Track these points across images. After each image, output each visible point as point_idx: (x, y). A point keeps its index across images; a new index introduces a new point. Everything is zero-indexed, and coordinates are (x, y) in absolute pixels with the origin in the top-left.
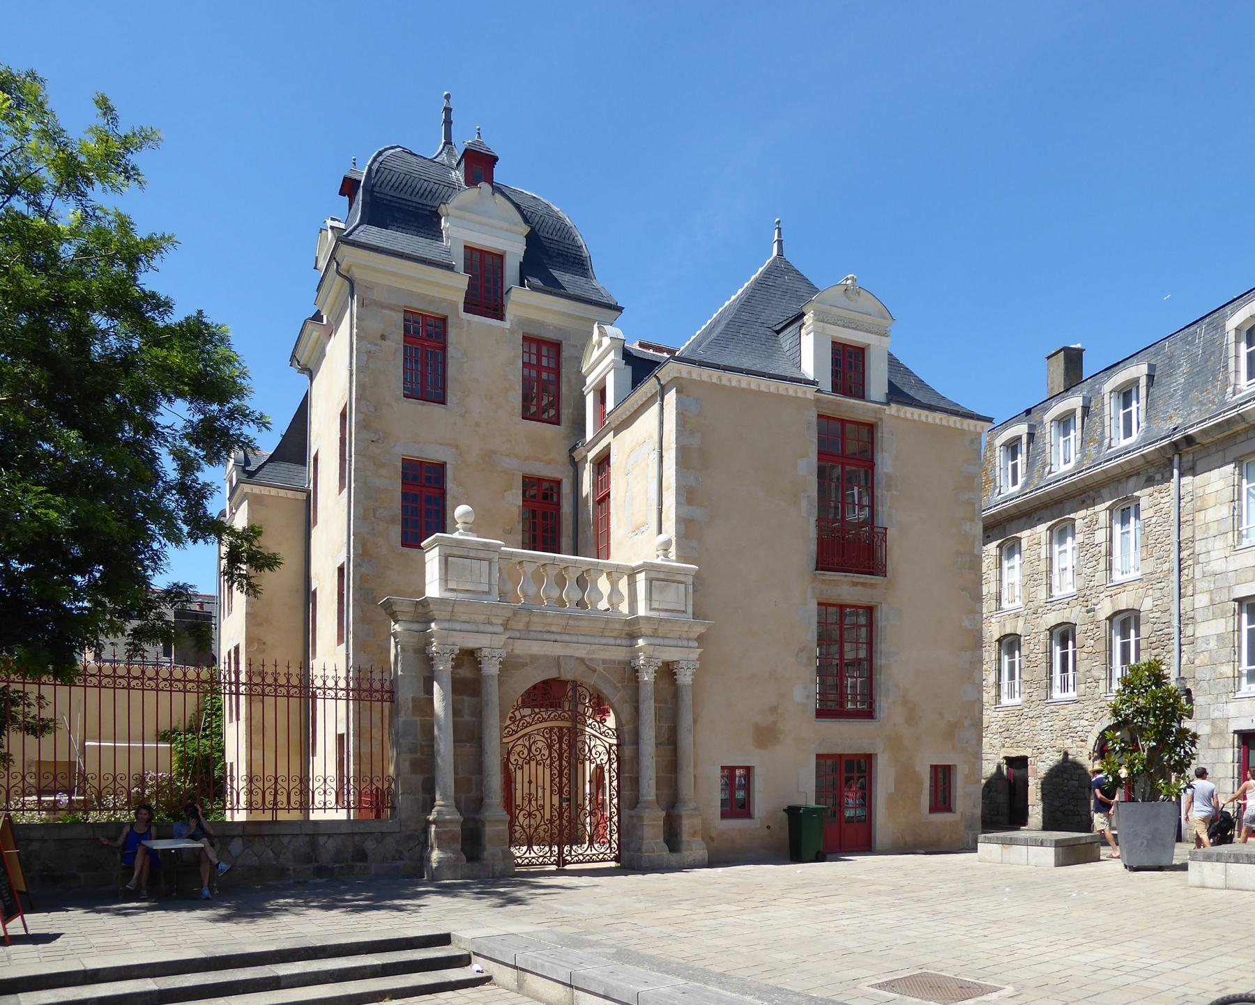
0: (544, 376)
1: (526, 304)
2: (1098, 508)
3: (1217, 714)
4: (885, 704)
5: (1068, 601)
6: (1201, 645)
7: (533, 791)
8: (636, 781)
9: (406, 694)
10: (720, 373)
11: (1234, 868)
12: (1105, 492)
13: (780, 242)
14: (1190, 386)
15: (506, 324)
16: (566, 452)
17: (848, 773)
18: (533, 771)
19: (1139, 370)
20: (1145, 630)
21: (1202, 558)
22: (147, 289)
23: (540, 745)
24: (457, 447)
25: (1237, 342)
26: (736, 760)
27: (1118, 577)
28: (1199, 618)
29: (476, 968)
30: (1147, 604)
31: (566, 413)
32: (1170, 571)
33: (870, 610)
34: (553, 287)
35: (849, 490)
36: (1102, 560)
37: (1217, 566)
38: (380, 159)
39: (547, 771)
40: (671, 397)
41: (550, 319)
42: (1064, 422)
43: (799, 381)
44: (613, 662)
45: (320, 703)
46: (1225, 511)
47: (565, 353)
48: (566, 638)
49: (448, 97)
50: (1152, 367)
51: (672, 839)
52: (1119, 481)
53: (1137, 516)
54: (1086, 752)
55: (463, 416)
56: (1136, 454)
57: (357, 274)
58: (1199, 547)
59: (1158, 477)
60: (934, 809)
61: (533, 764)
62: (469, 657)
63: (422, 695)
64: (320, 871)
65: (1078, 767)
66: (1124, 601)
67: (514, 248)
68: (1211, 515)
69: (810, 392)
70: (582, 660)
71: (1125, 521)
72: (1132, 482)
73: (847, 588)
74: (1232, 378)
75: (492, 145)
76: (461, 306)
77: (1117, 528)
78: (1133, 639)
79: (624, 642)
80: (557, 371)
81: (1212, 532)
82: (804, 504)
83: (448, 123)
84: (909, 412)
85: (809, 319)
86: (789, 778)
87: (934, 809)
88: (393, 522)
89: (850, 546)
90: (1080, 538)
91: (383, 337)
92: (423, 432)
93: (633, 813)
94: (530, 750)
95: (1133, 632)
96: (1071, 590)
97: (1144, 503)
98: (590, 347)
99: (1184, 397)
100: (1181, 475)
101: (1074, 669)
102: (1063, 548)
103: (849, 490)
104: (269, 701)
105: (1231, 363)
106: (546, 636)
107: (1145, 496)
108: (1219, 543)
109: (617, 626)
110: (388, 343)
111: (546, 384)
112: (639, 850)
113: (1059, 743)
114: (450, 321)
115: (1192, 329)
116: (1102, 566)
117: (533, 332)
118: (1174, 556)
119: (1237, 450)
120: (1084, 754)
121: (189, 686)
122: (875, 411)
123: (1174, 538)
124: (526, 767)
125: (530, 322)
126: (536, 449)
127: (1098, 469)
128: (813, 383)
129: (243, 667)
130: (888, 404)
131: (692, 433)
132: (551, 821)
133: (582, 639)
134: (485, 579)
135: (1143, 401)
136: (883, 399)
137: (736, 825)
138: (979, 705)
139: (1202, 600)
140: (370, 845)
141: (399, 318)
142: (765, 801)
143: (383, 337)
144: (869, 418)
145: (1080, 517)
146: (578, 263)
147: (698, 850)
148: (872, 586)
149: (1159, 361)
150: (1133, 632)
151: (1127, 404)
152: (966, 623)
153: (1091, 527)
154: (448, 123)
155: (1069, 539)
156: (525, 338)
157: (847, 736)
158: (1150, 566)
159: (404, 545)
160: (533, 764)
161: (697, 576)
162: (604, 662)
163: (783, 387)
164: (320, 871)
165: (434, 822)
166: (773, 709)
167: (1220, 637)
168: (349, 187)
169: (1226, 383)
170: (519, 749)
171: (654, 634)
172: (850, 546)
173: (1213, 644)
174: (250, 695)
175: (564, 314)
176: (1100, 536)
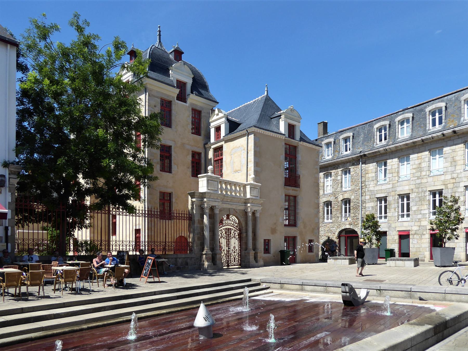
0: (196, 120)
1: (194, 99)
2: (338, 170)
5: (330, 195)
6: (367, 209)
8: (246, 244)
9: (197, 218)
10: (264, 131)
11: (397, 262)
12: (340, 166)
13: (267, 91)
14: (364, 140)
15: (187, 105)
16: (203, 145)
17: (291, 241)
19: (350, 134)
20: (352, 204)
21: (367, 186)
24: (175, 141)
25: (377, 132)
27: (344, 189)
28: (367, 202)
29: (263, 286)
30: (352, 197)
31: (203, 132)
32: (359, 189)
33: (295, 197)
34: (200, 95)
35: (290, 165)
36: (340, 184)
37: (371, 189)
38: (152, 50)
40: (252, 137)
41: (199, 104)
42: (328, 145)
43: (278, 133)
44: (241, 210)
46: (374, 175)
47: (203, 114)
48: (231, 203)
49: (159, 27)
50: (353, 134)
51: (256, 258)
52: (345, 163)
53: (350, 173)
54: (335, 237)
56: (350, 157)
57: (148, 86)
58: (367, 183)
59: (356, 164)
60: (309, 252)
62: (212, 209)
63: (201, 218)
64: (178, 268)
65: (332, 241)
66: (346, 196)
67: (189, 82)
68: (370, 175)
69: (283, 137)
70: (234, 209)
71: (346, 174)
72: (348, 164)
73: (291, 191)
74: (376, 140)
76: (176, 98)
77: (343, 176)
78: (348, 206)
79: (244, 204)
81: (371, 179)
84: (305, 144)
85: (283, 117)
86: (278, 244)
87: (309, 252)
88: (158, 163)
89: (292, 180)
90: (333, 178)
91: (155, 106)
93: (246, 252)
95: (348, 204)
96: (329, 192)
97: (351, 170)
98: (213, 115)
99: (363, 143)
100: (362, 164)
101: (331, 214)
102: (327, 180)
103: (290, 165)
105: (375, 136)
106: (227, 203)
107: (352, 168)
108: (372, 183)
109: (243, 200)
110: (156, 108)
111: (199, 124)
112: (249, 262)
113: (327, 234)
114: (173, 102)
115: (364, 125)
116: (340, 186)
117: (195, 107)
118: (360, 185)
119: (377, 159)
120: (334, 238)
122: (297, 143)
123: (360, 180)
125: (194, 104)
126: (195, 143)
127: (339, 160)
128: (284, 135)
129: (146, 209)
130: (300, 141)
131: (257, 147)
132: (226, 254)
133: (234, 203)
135: (351, 143)
136: (299, 140)
137: (267, 255)
138: (318, 223)
139: (367, 197)
140: (189, 261)
141: (159, 100)
142: (274, 248)
143: (155, 106)
144: (295, 145)
145: (333, 172)
146: (205, 87)
147: (261, 262)
148: (297, 191)
149: (355, 132)
150: (348, 204)
151: (346, 142)
152: (316, 201)
153: (336, 175)
155: (329, 178)
156: (192, 109)
158: (353, 187)
159: (161, 171)
161: (261, 187)
162: (239, 210)
163: (271, 134)
164: (178, 268)
165: (205, 254)
166: (275, 224)
167: (372, 207)
169: (374, 142)
171: (252, 203)
172: (292, 180)
173: (370, 209)
174: (148, 217)
175: (204, 103)
176: (339, 178)
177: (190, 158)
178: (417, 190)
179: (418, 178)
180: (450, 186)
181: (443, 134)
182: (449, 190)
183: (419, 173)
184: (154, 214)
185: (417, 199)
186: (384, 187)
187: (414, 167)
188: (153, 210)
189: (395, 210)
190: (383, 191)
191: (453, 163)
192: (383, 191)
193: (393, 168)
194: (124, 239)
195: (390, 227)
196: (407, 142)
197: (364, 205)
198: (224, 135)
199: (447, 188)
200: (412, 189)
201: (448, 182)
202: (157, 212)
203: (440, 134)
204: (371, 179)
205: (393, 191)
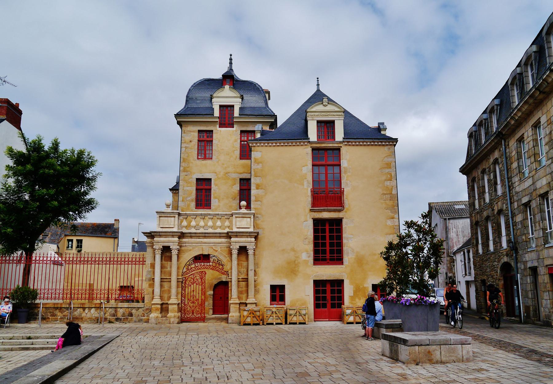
7: (195, 294)
22: (63, 150)
23: (198, 278)
26: (277, 282)
39: (200, 287)
45: (33, 265)
55: (218, 162)
61: (195, 284)
64: (118, 320)
88: (192, 201)
92: (203, 169)
94: (194, 280)
104: (11, 265)
124: (192, 286)
134: (172, 223)
140: (134, 311)
143: (191, 141)
157: (328, 272)
160: (195, 284)
170: (189, 279)
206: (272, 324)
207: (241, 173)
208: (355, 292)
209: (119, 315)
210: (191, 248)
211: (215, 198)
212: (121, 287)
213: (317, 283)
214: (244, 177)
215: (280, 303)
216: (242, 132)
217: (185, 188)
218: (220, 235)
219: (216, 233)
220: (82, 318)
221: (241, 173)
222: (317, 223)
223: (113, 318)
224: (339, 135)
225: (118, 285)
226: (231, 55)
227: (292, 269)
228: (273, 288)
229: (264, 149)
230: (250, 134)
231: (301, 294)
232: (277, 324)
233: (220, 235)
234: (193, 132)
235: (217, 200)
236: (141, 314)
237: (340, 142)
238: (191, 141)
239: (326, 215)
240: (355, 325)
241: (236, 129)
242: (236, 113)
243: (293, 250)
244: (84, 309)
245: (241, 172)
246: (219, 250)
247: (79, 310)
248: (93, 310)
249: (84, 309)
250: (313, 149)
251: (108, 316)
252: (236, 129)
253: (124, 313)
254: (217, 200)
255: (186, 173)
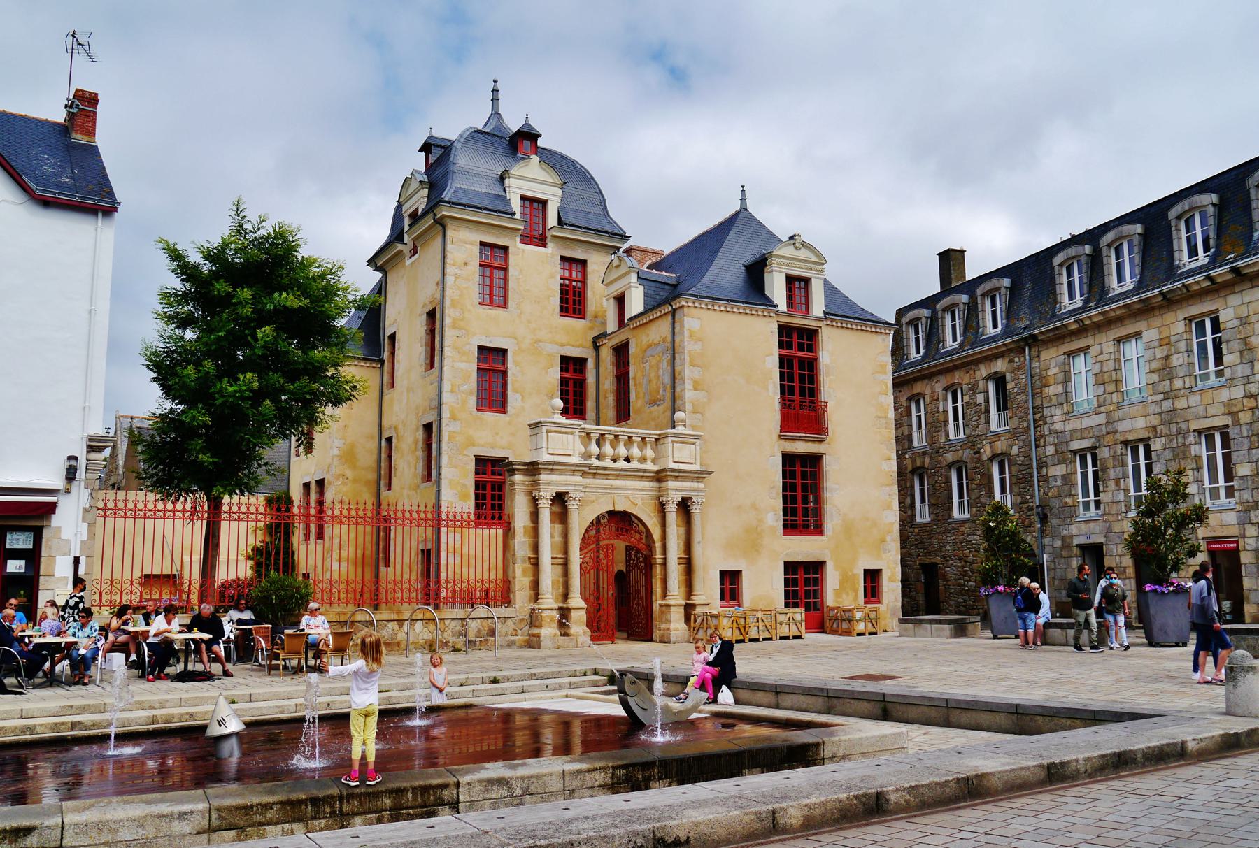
3: (1065, 533)
4: (831, 523)
18: (472, 571)
37: (1058, 427)
55: (519, 316)
58: (1046, 412)
64: (472, 643)
75: (537, 125)
80: (584, 282)
81: (1054, 402)
82: (771, 387)
83: (495, 100)
88: (471, 394)
108: (1058, 411)
116: (983, 421)
121: (149, 514)
134: (571, 447)
143: (466, 264)
154: (495, 100)
157: (803, 548)
164: (472, 643)
168: (421, 150)
173: (1059, 482)
177: (555, 374)
178: (1165, 431)
179: (1168, 396)
180: (1245, 417)
181: (1208, 277)
182: (1244, 427)
183: (1168, 382)
184: (411, 519)
185: (1168, 455)
186: (1087, 422)
187: (1155, 365)
188: (422, 509)
189: (1117, 484)
190: (1086, 434)
191: (1247, 356)
192: (1086, 434)
193: (1105, 369)
194: (117, 576)
195: (1108, 532)
196: (1128, 301)
197: (1044, 471)
198: (641, 309)
199: (1236, 422)
200: (1154, 427)
201: (1239, 407)
202: (426, 512)
203: (1200, 277)
204: (1054, 402)
205: (1108, 433)
206: (757, 640)
207: (562, 345)
208: (842, 583)
209: (471, 635)
210: (594, 498)
211: (515, 391)
212: (146, 576)
213: (790, 567)
214: (568, 354)
215: (732, 603)
216: (563, 259)
217: (456, 365)
218: (642, 475)
219: (645, 471)
220: (398, 644)
221: (562, 345)
222: (788, 458)
223: (459, 642)
224: (818, 308)
225: (137, 574)
226: (495, 82)
227: (751, 542)
228: (723, 574)
229: (704, 314)
230: (574, 266)
231: (765, 586)
232: (764, 639)
233: (642, 475)
234: (471, 244)
235: (518, 396)
236: (510, 630)
237: (820, 320)
238: (466, 264)
239: (801, 447)
240: (867, 636)
241: (552, 252)
242: (552, 220)
243: (754, 507)
244: (400, 622)
245: (564, 341)
246: (640, 503)
247: (390, 625)
248: (419, 625)
249: (400, 622)
250: (784, 330)
251: (447, 636)
252: (552, 252)
253: (479, 631)
254: (518, 396)
255: (457, 333)
